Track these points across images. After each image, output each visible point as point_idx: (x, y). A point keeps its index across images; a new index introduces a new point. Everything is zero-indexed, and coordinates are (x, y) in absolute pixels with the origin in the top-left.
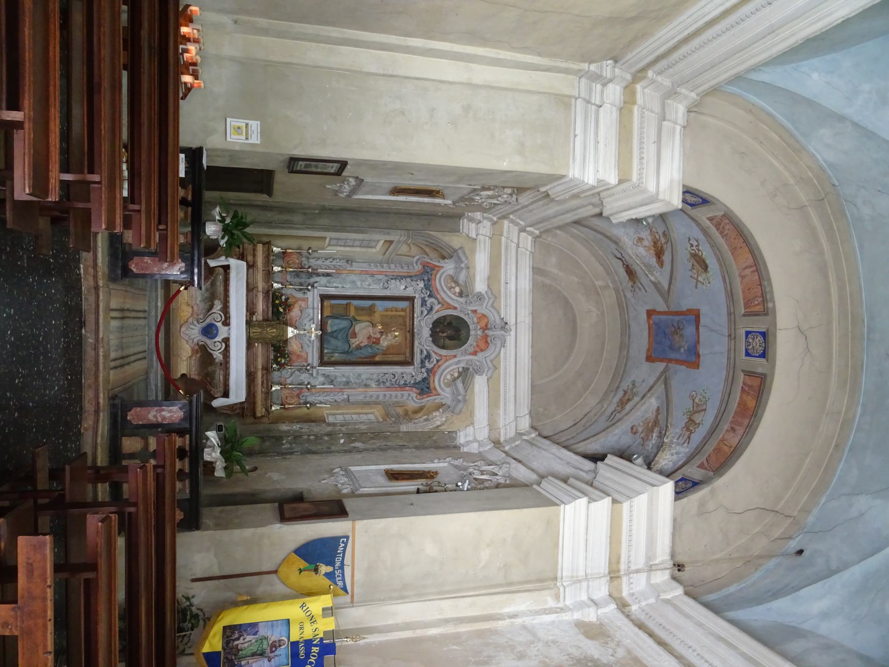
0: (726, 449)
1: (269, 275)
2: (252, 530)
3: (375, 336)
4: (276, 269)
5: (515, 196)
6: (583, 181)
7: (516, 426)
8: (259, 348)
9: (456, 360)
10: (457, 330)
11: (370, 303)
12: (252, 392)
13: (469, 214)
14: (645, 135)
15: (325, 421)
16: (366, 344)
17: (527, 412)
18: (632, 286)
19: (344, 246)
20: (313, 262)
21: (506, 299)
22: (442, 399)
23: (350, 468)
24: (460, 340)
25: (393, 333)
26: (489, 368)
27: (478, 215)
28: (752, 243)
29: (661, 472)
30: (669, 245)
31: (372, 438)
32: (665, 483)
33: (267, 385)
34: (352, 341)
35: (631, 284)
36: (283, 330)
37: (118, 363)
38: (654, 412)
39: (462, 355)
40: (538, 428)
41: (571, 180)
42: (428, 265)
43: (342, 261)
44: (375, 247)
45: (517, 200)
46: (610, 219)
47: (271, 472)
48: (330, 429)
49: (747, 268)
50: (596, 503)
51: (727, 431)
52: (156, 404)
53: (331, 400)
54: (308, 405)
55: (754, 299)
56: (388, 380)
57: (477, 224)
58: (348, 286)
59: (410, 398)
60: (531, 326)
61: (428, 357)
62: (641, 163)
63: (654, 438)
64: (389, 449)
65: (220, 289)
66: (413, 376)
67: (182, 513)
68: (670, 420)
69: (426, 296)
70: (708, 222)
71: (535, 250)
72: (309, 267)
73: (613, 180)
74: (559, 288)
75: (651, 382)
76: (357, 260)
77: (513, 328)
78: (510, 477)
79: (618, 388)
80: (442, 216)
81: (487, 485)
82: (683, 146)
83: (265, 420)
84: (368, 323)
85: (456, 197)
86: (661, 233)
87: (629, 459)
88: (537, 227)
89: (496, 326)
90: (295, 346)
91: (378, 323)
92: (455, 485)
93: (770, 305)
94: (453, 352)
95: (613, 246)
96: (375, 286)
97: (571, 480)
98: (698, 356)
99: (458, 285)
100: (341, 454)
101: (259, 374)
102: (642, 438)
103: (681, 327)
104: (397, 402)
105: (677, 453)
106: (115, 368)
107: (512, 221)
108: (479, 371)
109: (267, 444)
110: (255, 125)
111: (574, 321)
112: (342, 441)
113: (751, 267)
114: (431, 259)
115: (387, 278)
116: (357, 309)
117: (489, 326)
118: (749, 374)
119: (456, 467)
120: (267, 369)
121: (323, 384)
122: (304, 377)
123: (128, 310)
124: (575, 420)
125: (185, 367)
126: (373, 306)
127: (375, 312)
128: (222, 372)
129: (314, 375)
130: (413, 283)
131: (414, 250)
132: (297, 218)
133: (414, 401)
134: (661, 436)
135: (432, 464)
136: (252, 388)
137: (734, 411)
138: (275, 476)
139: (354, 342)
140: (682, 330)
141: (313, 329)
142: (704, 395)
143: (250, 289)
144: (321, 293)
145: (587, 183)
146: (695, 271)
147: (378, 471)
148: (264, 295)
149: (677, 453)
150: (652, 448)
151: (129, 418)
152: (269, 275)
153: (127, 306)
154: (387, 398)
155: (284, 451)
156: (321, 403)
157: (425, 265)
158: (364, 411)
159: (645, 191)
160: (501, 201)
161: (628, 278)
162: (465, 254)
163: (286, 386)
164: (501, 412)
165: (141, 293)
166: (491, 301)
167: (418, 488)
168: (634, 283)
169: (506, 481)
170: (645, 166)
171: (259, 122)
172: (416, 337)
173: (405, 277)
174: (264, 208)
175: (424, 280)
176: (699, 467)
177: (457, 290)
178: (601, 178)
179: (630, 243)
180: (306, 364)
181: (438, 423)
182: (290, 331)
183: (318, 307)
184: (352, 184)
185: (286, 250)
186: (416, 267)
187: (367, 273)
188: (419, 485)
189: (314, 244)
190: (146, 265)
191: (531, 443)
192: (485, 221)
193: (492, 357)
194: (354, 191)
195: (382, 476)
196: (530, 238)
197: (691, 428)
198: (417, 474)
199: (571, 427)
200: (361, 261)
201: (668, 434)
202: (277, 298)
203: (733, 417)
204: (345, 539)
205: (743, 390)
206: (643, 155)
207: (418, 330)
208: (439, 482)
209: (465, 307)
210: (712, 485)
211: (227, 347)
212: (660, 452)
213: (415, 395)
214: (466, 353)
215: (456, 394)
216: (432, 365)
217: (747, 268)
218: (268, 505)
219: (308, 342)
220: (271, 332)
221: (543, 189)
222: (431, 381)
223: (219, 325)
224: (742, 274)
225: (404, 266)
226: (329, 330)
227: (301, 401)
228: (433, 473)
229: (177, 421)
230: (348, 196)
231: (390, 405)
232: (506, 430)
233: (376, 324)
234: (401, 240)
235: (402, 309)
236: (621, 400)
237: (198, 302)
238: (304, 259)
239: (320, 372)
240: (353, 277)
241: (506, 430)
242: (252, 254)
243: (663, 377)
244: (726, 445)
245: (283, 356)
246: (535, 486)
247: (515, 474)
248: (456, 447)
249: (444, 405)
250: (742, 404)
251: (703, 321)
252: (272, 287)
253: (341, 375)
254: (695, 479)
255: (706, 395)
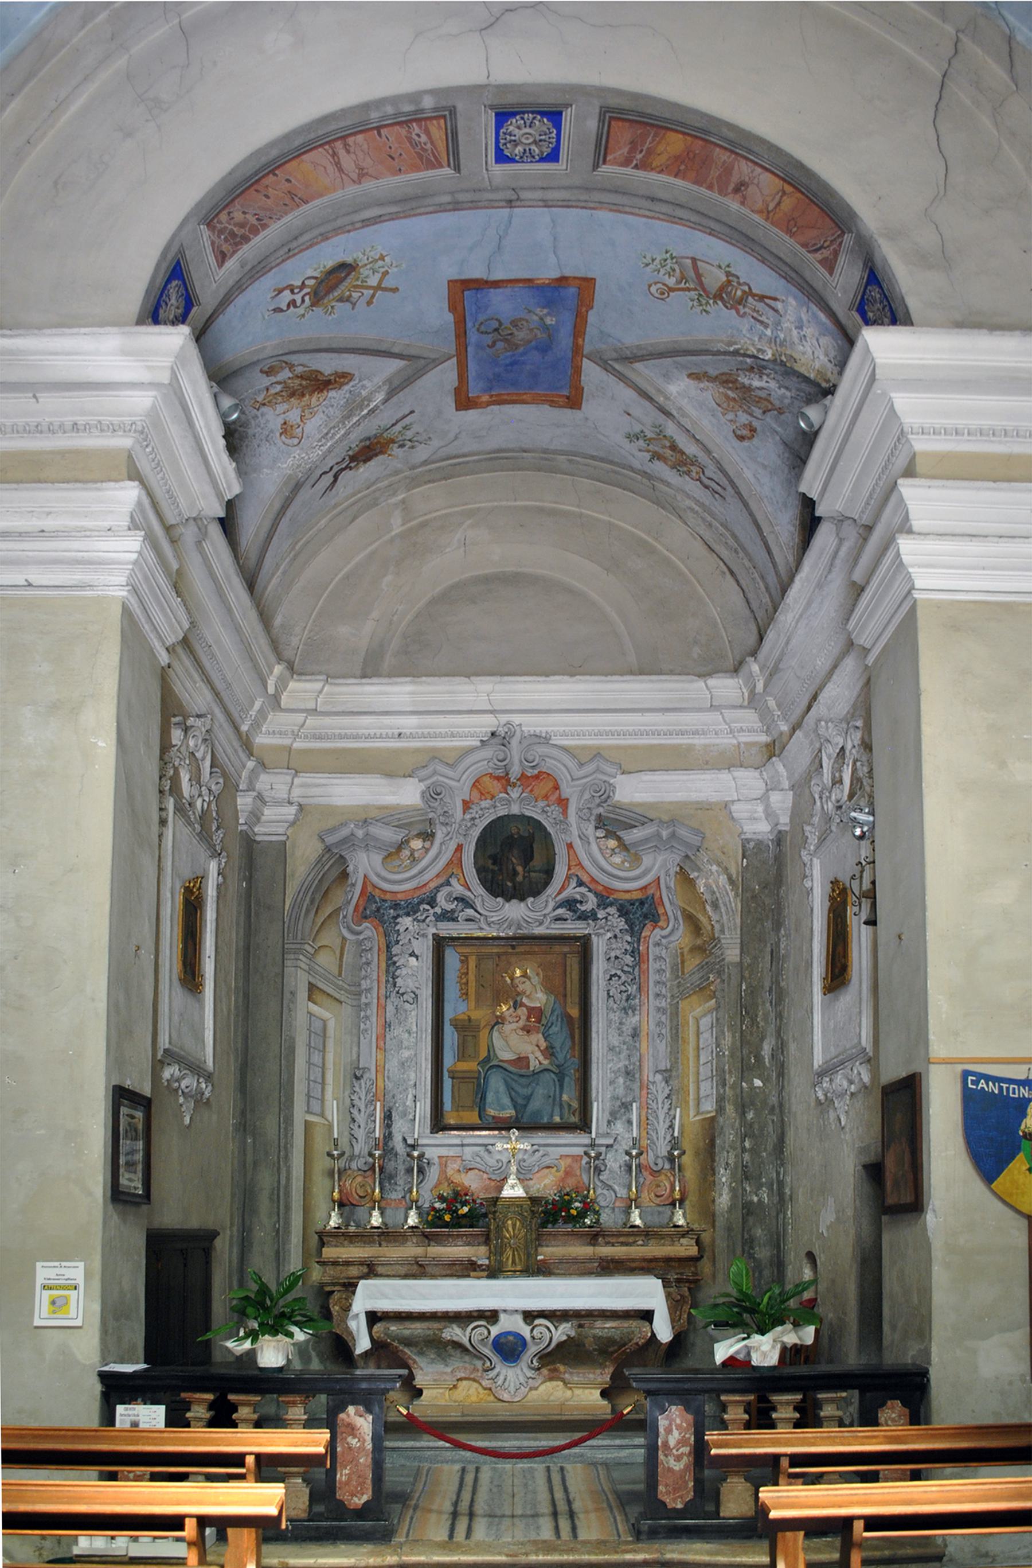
0: (787, 204)
1: (386, 1235)
2: (936, 1268)
3: (524, 1018)
4: (376, 1220)
5: (191, 721)
6: (135, 563)
7: (734, 707)
8: (546, 1252)
9: (577, 843)
10: (510, 842)
11: (448, 1031)
12: (644, 1264)
13: (241, 821)
14: (21, 421)
15: (713, 1119)
16: (540, 1035)
17: (701, 684)
18: (402, 446)
19: (323, 1083)
20: (361, 1147)
21: (436, 736)
22: (667, 874)
23: (816, 1066)
24: (531, 840)
25: (516, 981)
26: (598, 770)
27: (244, 802)
28: (274, 153)
29: (842, 364)
30: (293, 359)
31: (754, 1020)
32: (867, 350)
33: (628, 1235)
34: (534, 1065)
35: (395, 450)
36: (509, 1206)
37: (564, 1524)
38: (702, 385)
39: (565, 831)
40: (738, 658)
41: (135, 591)
42: (361, 909)
43: (357, 1089)
44: (325, 1022)
45: (199, 716)
46: (229, 501)
47: (818, 1226)
48: (730, 1109)
49: (338, 164)
50: (911, 517)
51: (743, 203)
52: (652, 1450)
53: (667, 1106)
54: (676, 1153)
55: (414, 144)
56: (623, 988)
57: (264, 803)
58: (412, 1076)
59: (664, 941)
60: (498, 679)
61: (570, 904)
62: (87, 428)
63: (763, 384)
64: (778, 983)
65: (417, 1329)
66: (615, 937)
67: (889, 1403)
68: (721, 347)
69: (432, 911)
70: (231, 264)
71: (320, 673)
72: (371, 1155)
73: (129, 494)
74: (409, 617)
75: (629, 394)
76: (355, 1057)
77: (504, 718)
78: (852, 715)
79: (645, 474)
80: (250, 880)
81: (866, 769)
82: (39, 328)
83: (706, 1237)
84: (495, 1034)
85: (203, 853)
86: (266, 381)
87: (809, 438)
88: (265, 670)
89: (501, 758)
90: (547, 1181)
91: (494, 1012)
92: (863, 843)
93: (428, 103)
94: (561, 851)
95: (305, 494)
96: (412, 1020)
97: (858, 576)
98: (562, 281)
99: (407, 842)
100: (786, 1083)
101: (606, 1251)
102: (764, 412)
103: (496, 325)
104: (674, 969)
105: (800, 327)
106: (574, 1529)
107: (257, 725)
108: (604, 794)
109: (758, 1232)
110: (44, 1272)
111: (486, 580)
112: (758, 1083)
113: (334, 154)
114: (349, 902)
115: (393, 994)
116: (462, 1055)
117: (500, 773)
118: (601, 153)
119: (822, 840)
120: (595, 1236)
121: (630, 1122)
122: (614, 1161)
123: (456, 1504)
124: (724, 573)
125: (587, 1391)
126: (456, 1024)
127: (470, 1020)
128: (599, 1324)
129: (610, 1141)
130: (404, 939)
131: (328, 938)
132: (265, 1180)
133: (670, 934)
134: (759, 367)
135: (815, 891)
136: (634, 1265)
137: (695, 188)
138: (828, 1217)
139: (537, 1060)
140: (501, 324)
141: (509, 1146)
142: (657, 262)
143: (419, 1270)
144: (428, 1131)
145: (140, 553)
146: (355, 295)
147: (825, 1007)
148: (433, 1243)
149: (800, 327)
150: (787, 388)
151: (680, 1506)
152: (386, 1235)
153: (448, 1507)
154: (664, 991)
155: (776, 1199)
156: (671, 1127)
157: (363, 916)
158: (692, 1038)
159: (153, 414)
160: (205, 752)
161: (381, 457)
162: (333, 830)
163: (633, 1197)
164: (698, 741)
165: (423, 1479)
166: (441, 768)
167: (865, 923)
168: (393, 441)
169: (857, 727)
170: (92, 419)
171: (39, 1265)
172: (526, 931)
173: (390, 957)
174: (245, 1244)
175: (396, 918)
176: (831, 272)
177: (417, 844)
178: (125, 522)
179: (297, 452)
180: (585, 1159)
181: (723, 879)
182: (511, 1192)
183: (459, 1136)
184: (177, 1072)
185: (334, 1201)
186: (368, 933)
187: (382, 1037)
188: (860, 919)
189: (321, 1145)
190: (354, 1477)
191: (773, 673)
192: (258, 786)
193: (571, 764)
194: (195, 1068)
195: (837, 999)
196: (292, 685)
197: (739, 293)
198: (836, 925)
199: (737, 581)
200: (355, 1049)
201: (753, 351)
202: (440, 1218)
203: (710, 187)
204: (970, 1078)
205: (640, 166)
206: (68, 425)
207: (509, 927)
208: (853, 877)
209: (455, 826)
210: (876, 236)
211: (542, 1314)
212: (797, 367)
213: (657, 930)
214: (563, 822)
215: (657, 844)
216: (591, 895)
217: (338, 164)
218: (886, 1238)
219: (538, 1155)
220: (512, 1229)
221: (164, 658)
222: (627, 896)
223: (495, 1331)
224: (355, 176)
225: (364, 960)
226: (509, 1112)
227: (667, 1166)
228: (833, 891)
229: (690, 1417)
230: (209, 1077)
231: (679, 985)
232: (742, 730)
233: (497, 1017)
234: (306, 967)
235: (462, 961)
236: (673, 467)
237: (449, 1370)
238: (354, 1166)
239: (604, 1128)
240: (393, 1065)
241: (742, 730)
242: (344, 1268)
243: (617, 366)
244: (779, 204)
245: (567, 1205)
246: (870, 660)
247: (843, 708)
248: (780, 839)
249: (681, 868)
250: (678, 166)
251: (477, 273)
252: (416, 1227)
253: (611, 1088)
254: (862, 278)
255: (658, 259)
